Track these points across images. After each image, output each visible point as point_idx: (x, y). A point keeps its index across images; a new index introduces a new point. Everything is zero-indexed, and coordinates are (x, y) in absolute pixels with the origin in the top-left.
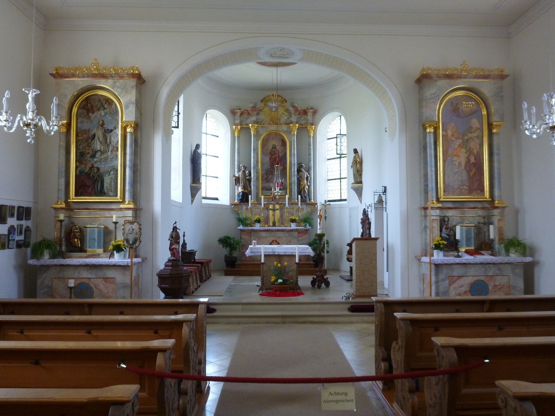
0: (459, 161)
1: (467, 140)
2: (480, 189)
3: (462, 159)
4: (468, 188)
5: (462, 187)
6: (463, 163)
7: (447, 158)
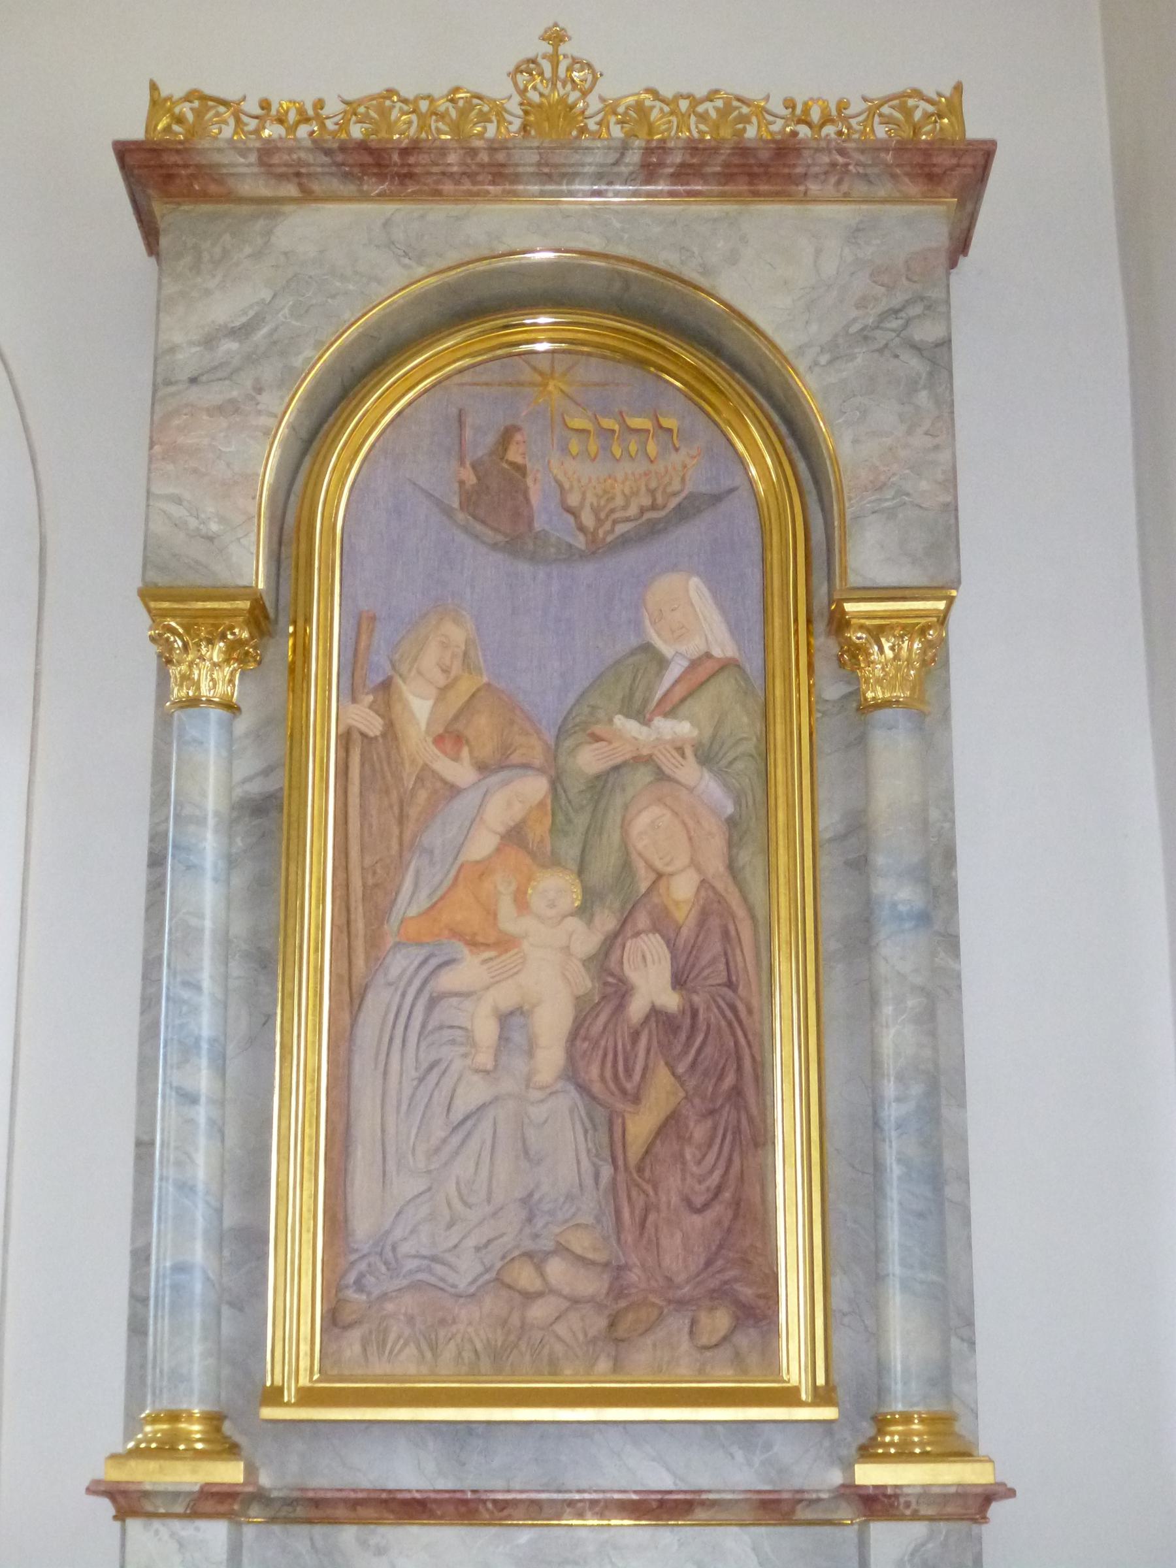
0: (504, 996)
1: (601, 785)
2: (720, 1294)
3: (544, 958)
4: (591, 1285)
5: (526, 1277)
6: (552, 1022)
7: (376, 961)
